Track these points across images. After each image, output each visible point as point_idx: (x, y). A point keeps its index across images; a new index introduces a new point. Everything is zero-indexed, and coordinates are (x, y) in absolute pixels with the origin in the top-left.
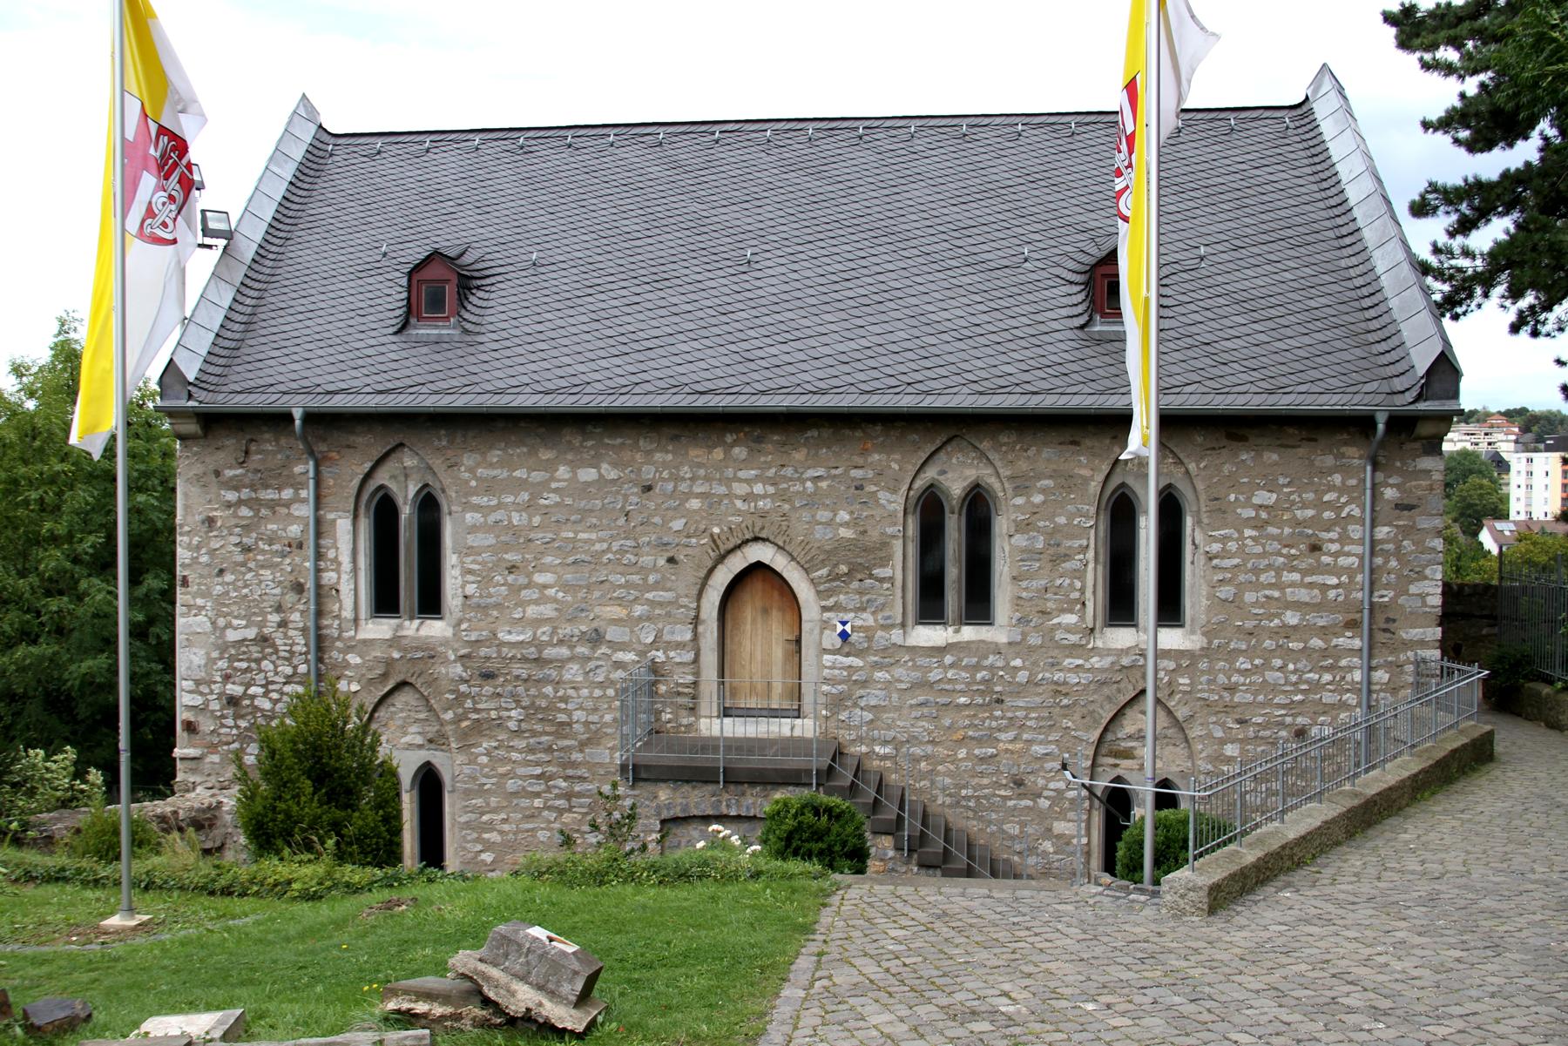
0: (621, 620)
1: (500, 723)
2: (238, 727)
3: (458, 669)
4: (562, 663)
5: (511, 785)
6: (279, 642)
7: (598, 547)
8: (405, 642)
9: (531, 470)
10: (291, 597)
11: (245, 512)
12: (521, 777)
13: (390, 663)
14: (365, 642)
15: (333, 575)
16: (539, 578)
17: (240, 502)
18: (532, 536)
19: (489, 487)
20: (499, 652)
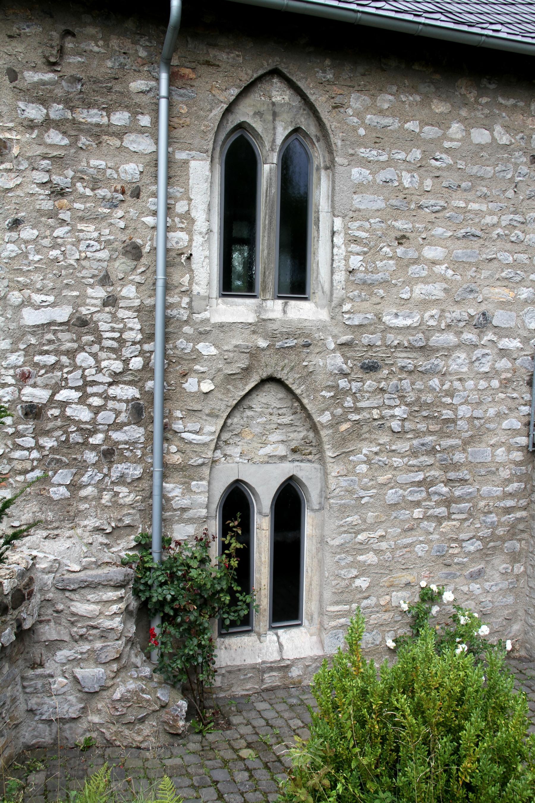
0: (508, 303)
1: (381, 424)
2: (39, 448)
3: (339, 360)
4: (448, 351)
5: (392, 496)
6: (103, 326)
7: (489, 220)
8: (271, 326)
9: (423, 123)
10: (121, 265)
11: (55, 137)
12: (402, 486)
13: (254, 354)
14: (221, 326)
15: (183, 236)
16: (429, 253)
17: (48, 123)
18: (423, 202)
19: (378, 139)
20: (383, 339)
